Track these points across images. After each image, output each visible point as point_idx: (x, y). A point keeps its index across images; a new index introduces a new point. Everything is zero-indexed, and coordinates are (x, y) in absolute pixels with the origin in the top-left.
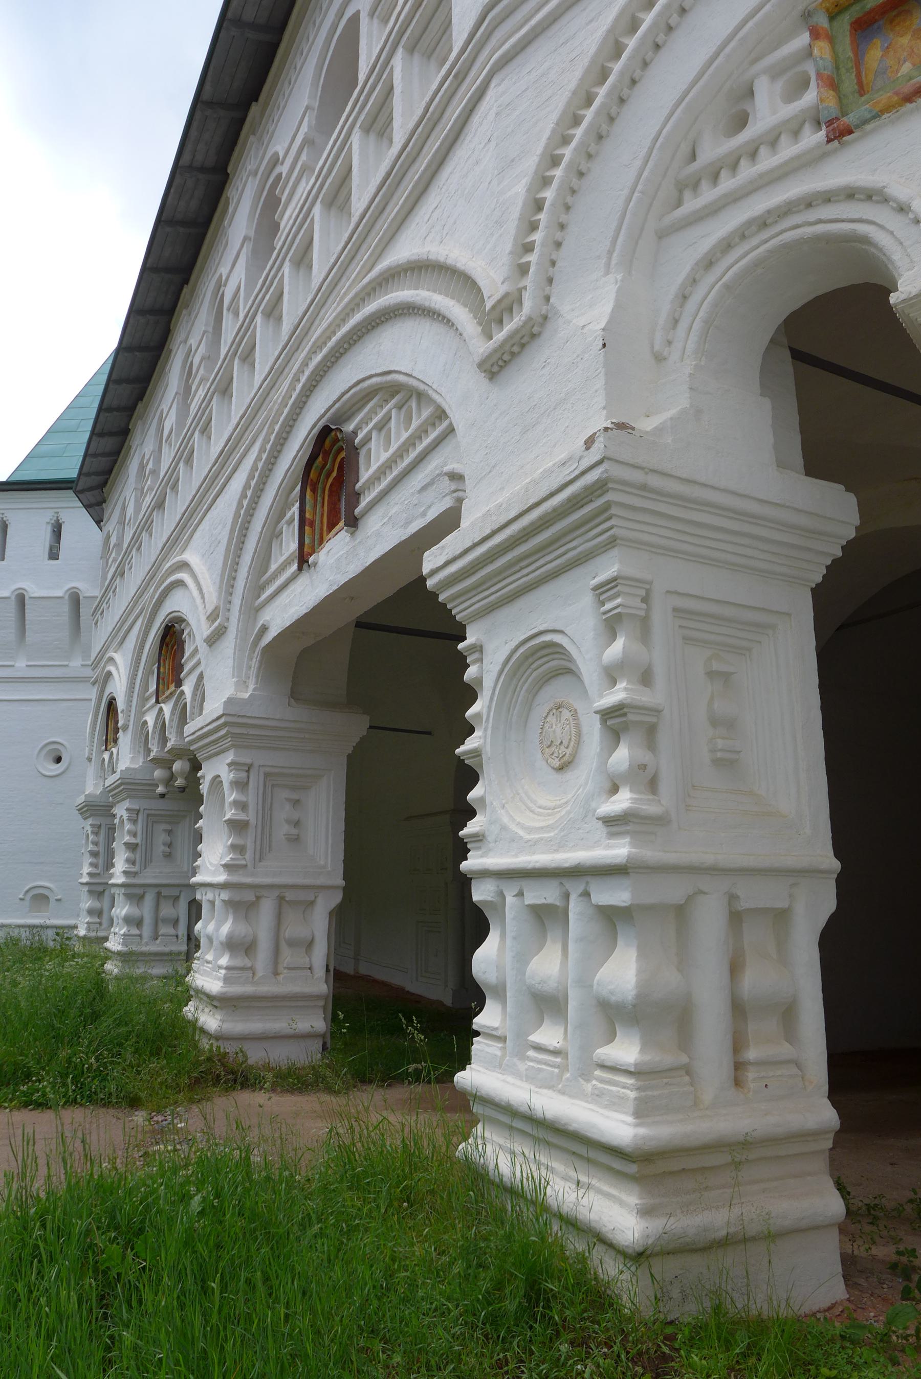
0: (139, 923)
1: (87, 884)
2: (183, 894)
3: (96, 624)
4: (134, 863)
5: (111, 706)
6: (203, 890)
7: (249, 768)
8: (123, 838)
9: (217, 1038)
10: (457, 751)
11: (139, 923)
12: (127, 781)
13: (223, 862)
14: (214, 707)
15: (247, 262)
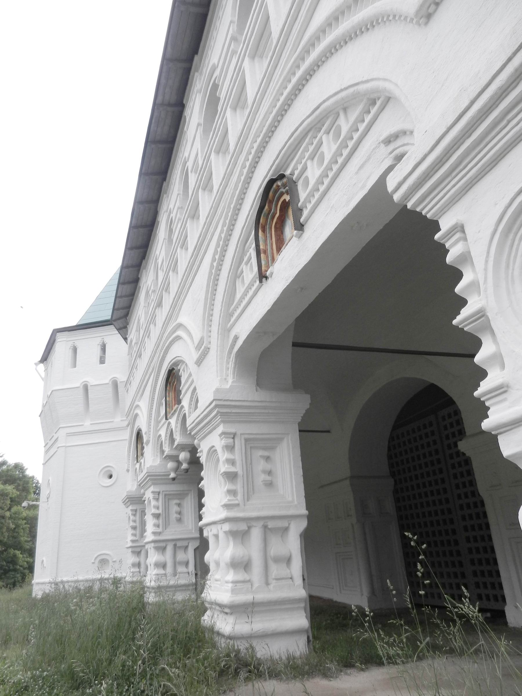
0: (164, 566)
1: (131, 547)
2: (190, 544)
3: (127, 391)
4: (158, 526)
5: (139, 435)
6: (209, 528)
8: (150, 511)
9: (230, 638)
10: (454, 322)
11: (164, 566)
13: (223, 503)
14: (206, 398)
15: (201, 137)
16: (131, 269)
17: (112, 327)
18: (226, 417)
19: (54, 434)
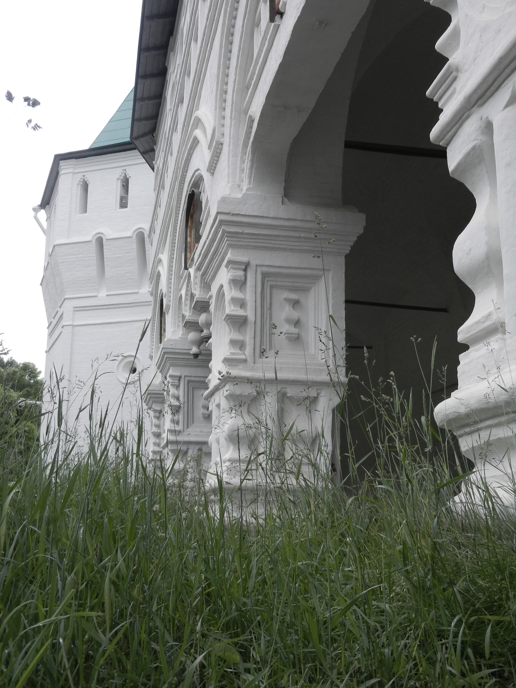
7: (246, 267)
12: (168, 350)
16: (153, 52)
17: (136, 153)
18: (236, 239)
19: (58, 309)
